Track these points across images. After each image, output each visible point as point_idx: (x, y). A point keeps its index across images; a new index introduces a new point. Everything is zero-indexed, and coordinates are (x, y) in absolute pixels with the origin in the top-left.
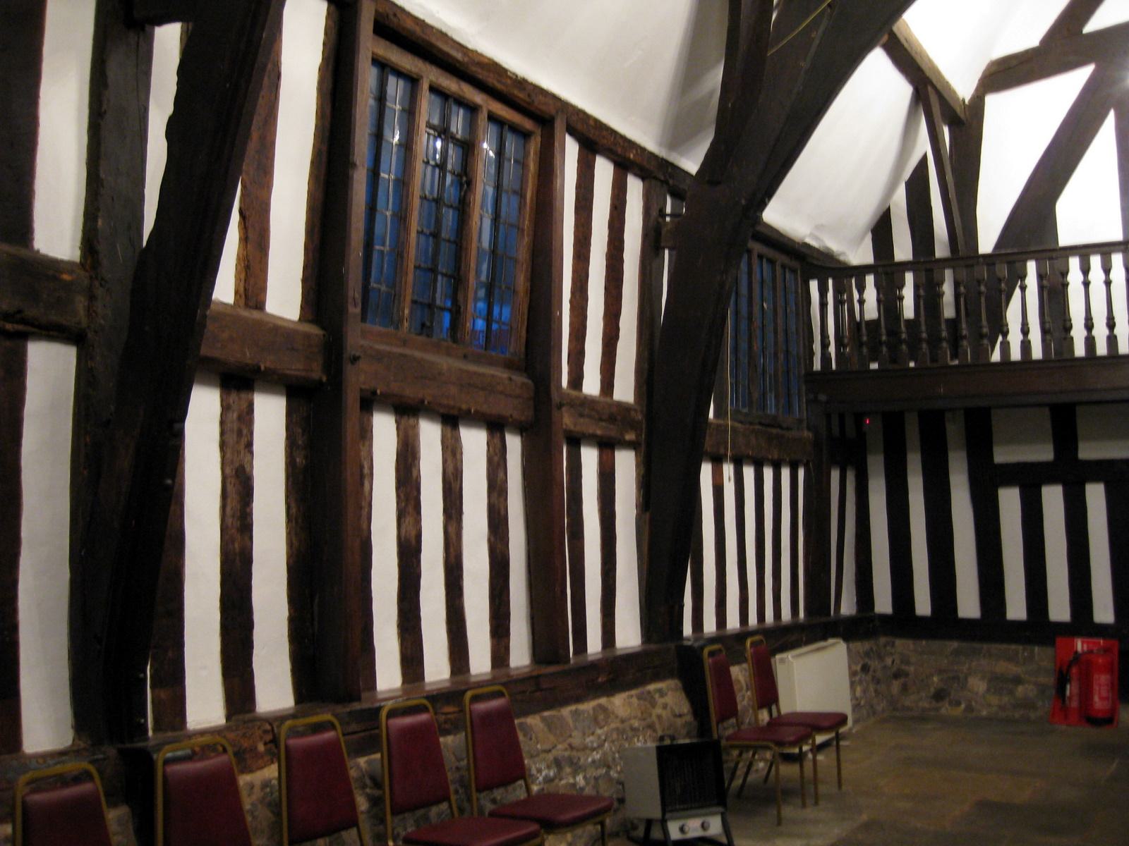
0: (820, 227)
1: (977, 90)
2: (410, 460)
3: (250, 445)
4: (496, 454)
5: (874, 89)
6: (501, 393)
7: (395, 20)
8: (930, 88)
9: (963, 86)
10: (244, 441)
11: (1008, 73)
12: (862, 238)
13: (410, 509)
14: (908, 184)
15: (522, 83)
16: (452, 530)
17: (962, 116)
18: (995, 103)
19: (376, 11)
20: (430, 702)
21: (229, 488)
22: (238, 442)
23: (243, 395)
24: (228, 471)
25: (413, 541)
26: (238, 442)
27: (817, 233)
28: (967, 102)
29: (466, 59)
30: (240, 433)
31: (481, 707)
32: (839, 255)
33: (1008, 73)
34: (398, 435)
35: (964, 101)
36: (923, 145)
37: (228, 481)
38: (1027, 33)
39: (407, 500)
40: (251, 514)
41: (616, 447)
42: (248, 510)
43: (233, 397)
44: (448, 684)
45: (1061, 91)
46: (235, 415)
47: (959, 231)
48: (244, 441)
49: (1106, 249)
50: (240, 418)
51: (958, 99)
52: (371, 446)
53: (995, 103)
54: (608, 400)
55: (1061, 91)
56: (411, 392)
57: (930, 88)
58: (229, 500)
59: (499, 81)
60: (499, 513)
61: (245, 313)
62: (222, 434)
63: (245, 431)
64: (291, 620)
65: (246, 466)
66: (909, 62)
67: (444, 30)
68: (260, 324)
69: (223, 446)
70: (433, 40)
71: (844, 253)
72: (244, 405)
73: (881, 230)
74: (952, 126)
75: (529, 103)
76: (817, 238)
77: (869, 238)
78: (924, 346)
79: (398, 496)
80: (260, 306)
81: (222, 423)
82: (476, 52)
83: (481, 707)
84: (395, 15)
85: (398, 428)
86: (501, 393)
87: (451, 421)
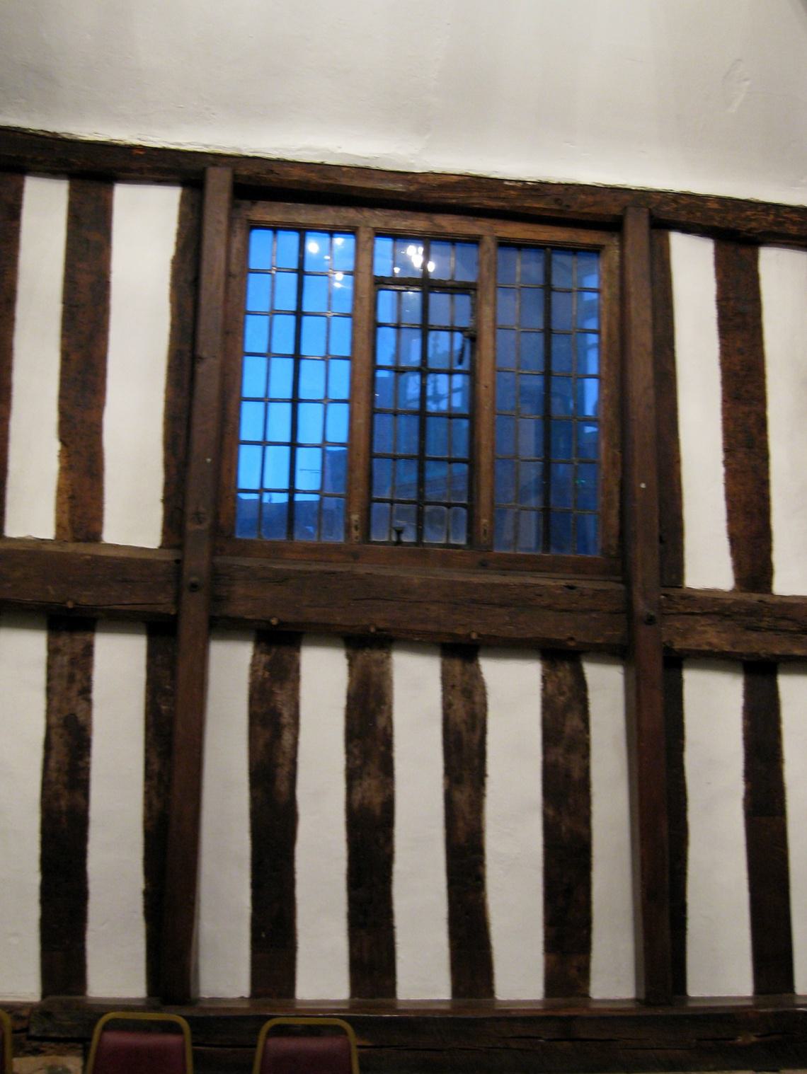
2: (372, 705)
3: (86, 691)
4: (563, 694)
6: (548, 607)
7: (271, 176)
10: (77, 687)
13: (373, 767)
15: (541, 188)
16: (461, 797)
19: (235, 176)
20: (191, 1026)
21: (55, 738)
22: (68, 689)
23: (79, 637)
24: (54, 720)
25: (378, 811)
26: (68, 689)
29: (412, 188)
30: (71, 679)
31: (113, 1038)
34: (351, 674)
37: (53, 732)
39: (366, 755)
40: (86, 770)
41: (685, 663)
43: (64, 640)
44: (246, 1005)
46: (66, 659)
48: (77, 687)
50: (73, 662)
52: (296, 690)
54: (755, 597)
56: (378, 619)
58: (54, 755)
59: (490, 198)
60: (568, 776)
61: (71, 547)
62: (50, 678)
63: (78, 677)
64: (146, 894)
65: (78, 715)
67: (361, 164)
68: (97, 561)
69: (50, 690)
70: (345, 182)
72: (78, 648)
75: (560, 211)
79: (349, 752)
80: (94, 535)
81: (50, 667)
82: (546, 184)
83: (113, 1038)
84: (272, 172)
85: (351, 665)
86: (548, 607)
87: (368, 644)
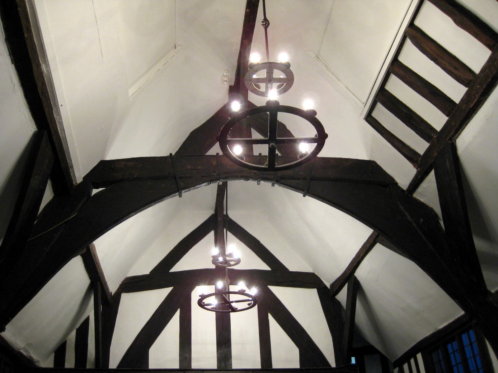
0: (29, 345)
1: (118, 289)
5: (74, 273)
8: (99, 283)
9: (113, 287)
11: (134, 284)
12: (49, 355)
14: (77, 330)
17: (110, 300)
18: (125, 297)
27: (27, 348)
28: (112, 295)
32: (36, 362)
33: (134, 284)
35: (111, 293)
36: (90, 312)
38: (145, 267)
42: (402, 189)
45: (156, 297)
47: (101, 353)
49: (460, 115)
51: (109, 291)
53: (125, 297)
55: (156, 297)
57: (99, 283)
66: (92, 267)
68: (78, 253)
71: (38, 362)
73: (60, 352)
74: (105, 302)
76: (27, 351)
77: (53, 355)
78: (453, 132)
